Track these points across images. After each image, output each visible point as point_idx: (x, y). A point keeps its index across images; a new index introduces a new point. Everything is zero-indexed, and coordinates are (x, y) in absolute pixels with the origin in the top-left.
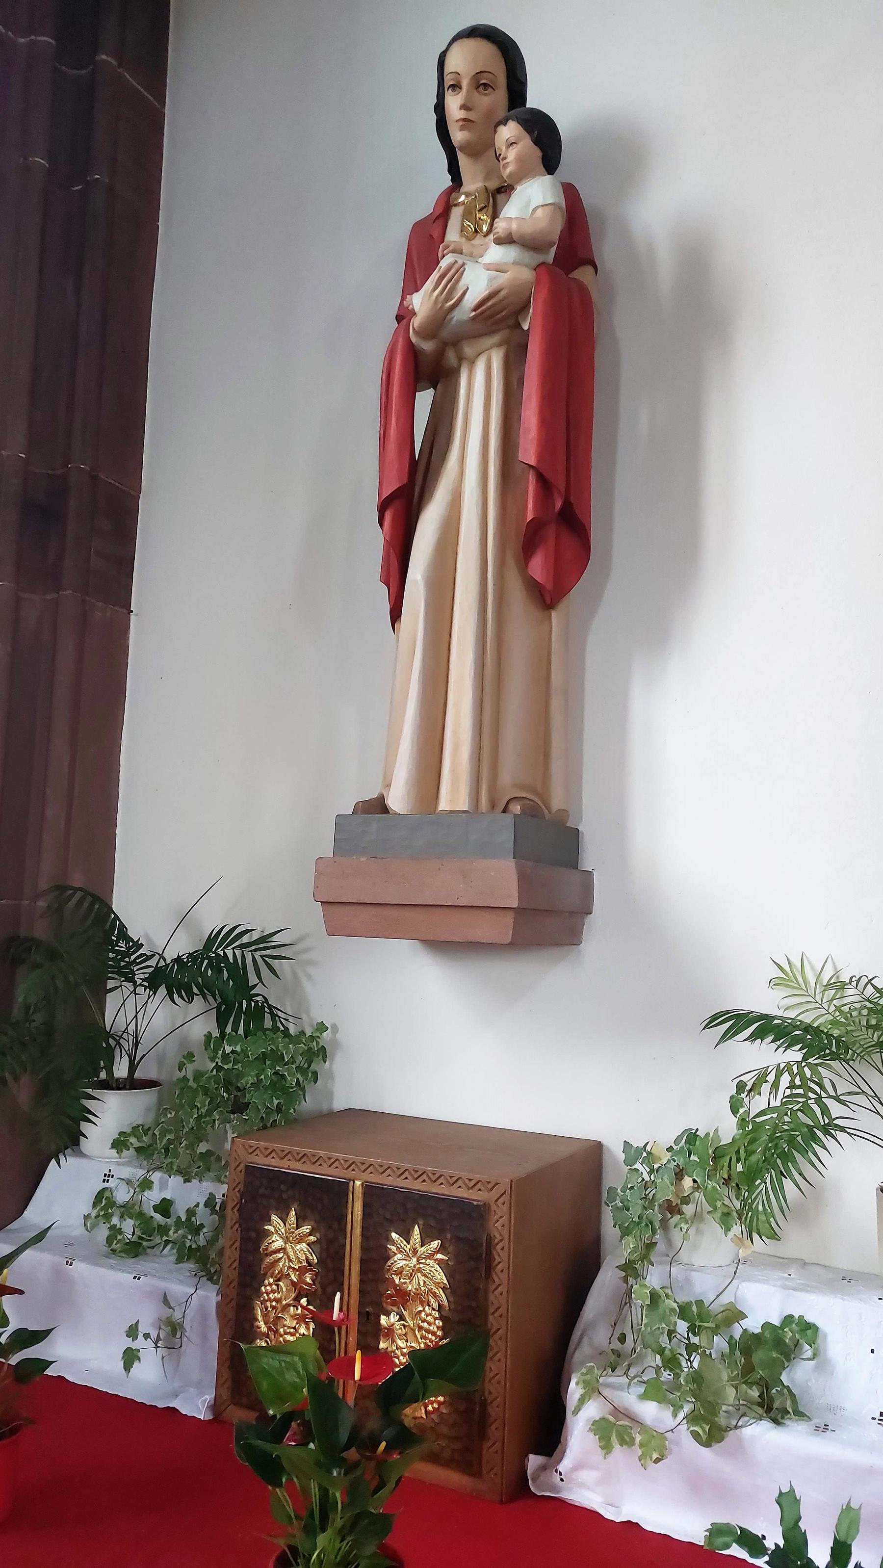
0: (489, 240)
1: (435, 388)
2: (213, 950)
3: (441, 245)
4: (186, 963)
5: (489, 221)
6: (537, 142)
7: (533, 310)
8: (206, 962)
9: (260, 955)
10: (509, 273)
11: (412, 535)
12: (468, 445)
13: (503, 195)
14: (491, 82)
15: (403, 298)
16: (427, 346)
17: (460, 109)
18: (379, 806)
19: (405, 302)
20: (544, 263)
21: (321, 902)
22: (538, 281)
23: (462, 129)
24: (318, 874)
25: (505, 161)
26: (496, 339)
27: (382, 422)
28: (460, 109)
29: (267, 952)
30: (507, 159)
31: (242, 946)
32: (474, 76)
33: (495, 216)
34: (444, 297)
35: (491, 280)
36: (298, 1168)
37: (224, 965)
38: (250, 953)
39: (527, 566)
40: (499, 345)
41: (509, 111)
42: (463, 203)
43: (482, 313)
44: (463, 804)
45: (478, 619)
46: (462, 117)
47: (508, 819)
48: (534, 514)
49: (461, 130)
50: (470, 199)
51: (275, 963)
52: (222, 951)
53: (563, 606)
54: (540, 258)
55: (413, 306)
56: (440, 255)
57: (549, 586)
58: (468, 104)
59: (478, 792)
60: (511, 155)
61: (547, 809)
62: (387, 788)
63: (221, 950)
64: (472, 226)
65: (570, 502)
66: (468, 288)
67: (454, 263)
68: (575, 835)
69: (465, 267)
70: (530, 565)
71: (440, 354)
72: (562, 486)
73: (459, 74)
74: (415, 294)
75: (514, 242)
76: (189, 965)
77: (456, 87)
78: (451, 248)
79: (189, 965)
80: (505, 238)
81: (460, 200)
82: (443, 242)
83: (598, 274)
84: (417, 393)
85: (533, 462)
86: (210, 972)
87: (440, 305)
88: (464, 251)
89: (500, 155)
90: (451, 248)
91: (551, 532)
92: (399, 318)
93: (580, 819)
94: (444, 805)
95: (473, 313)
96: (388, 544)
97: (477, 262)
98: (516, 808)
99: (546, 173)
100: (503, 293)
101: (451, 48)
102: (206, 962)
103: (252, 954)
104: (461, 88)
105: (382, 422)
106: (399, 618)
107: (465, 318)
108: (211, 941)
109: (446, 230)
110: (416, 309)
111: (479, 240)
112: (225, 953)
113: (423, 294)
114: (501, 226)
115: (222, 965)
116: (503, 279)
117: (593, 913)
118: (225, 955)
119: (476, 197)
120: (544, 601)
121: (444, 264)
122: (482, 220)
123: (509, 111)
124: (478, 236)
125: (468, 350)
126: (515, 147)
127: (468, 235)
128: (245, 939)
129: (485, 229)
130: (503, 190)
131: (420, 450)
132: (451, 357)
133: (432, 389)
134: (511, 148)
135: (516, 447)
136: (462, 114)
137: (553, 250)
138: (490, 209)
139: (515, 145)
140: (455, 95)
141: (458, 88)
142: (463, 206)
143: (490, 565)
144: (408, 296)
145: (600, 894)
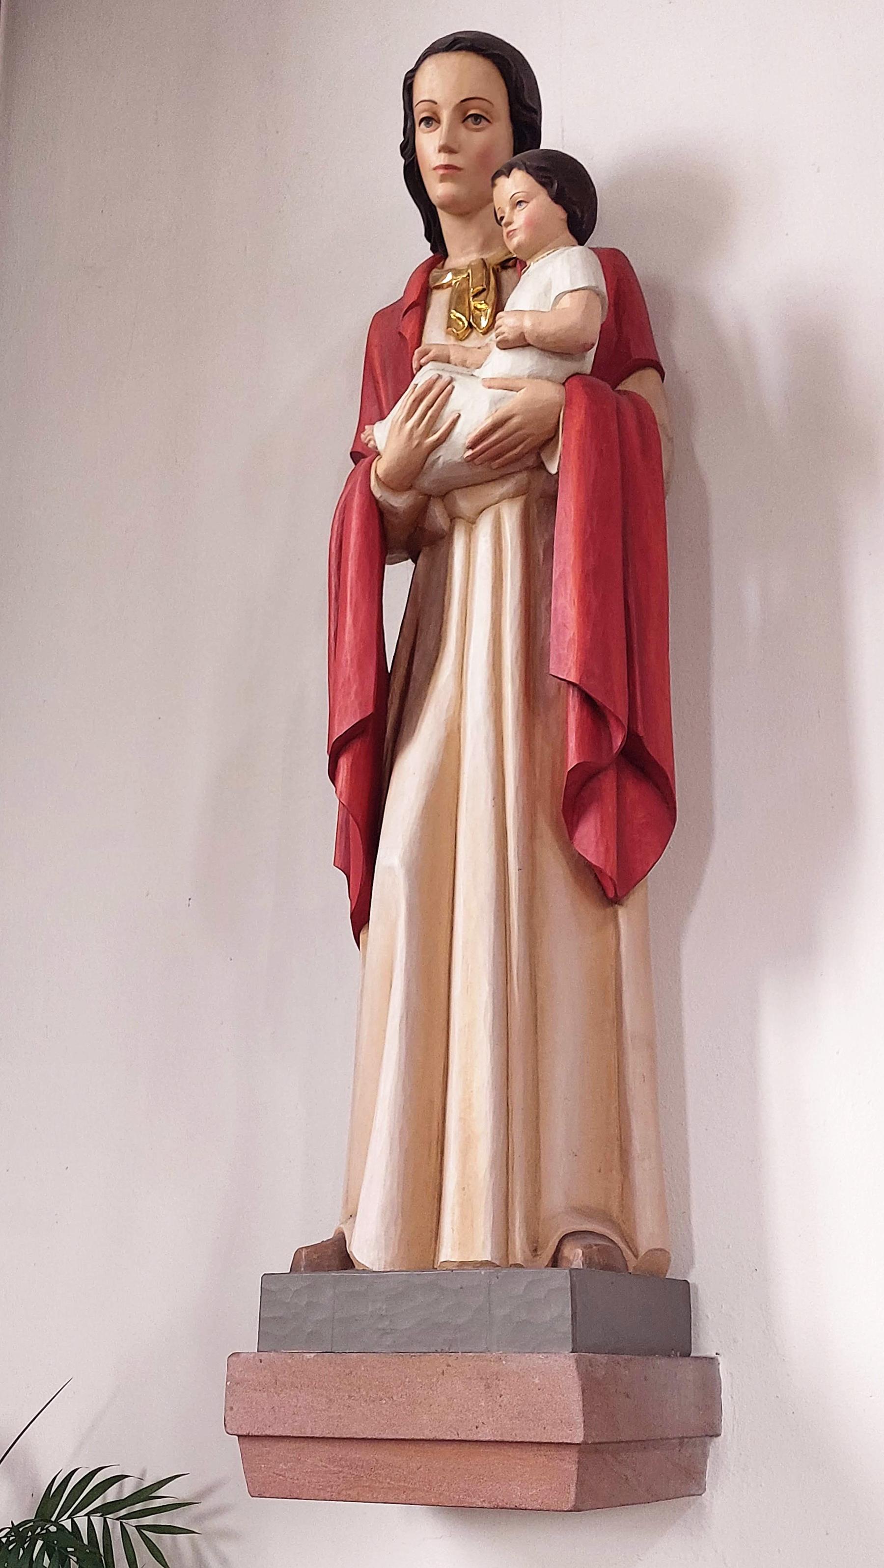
0: (491, 340)
1: (415, 561)
2: (53, 1519)
3: (416, 351)
4: (6, 1546)
5: (489, 311)
6: (557, 198)
7: (563, 446)
8: (40, 1543)
9: (136, 1527)
10: (523, 391)
11: (385, 792)
12: (469, 649)
13: (510, 271)
14: (487, 113)
15: (360, 429)
16: (400, 502)
17: (440, 151)
18: (339, 1245)
19: (362, 436)
20: (577, 374)
21: (239, 1436)
22: (569, 402)
23: (443, 179)
24: (233, 1385)
25: (510, 228)
26: (507, 487)
27: (332, 616)
28: (440, 151)
29: (148, 1520)
30: (513, 225)
31: (106, 1510)
32: (457, 105)
33: (499, 306)
34: (423, 430)
35: (495, 402)
36: (412, 1437)
37: (72, 1550)
38: (118, 1522)
39: (571, 837)
40: (513, 496)
41: (515, 154)
42: (449, 285)
43: (483, 452)
44: (483, 1250)
45: (495, 930)
46: (442, 163)
47: (560, 1278)
48: (579, 758)
49: (441, 181)
50: (460, 278)
51: (164, 1541)
52: (70, 1520)
53: (635, 898)
54: (572, 367)
55: (375, 441)
56: (415, 366)
57: (610, 869)
58: (454, 146)
59: (508, 1229)
60: (520, 218)
61: (630, 1249)
62: (351, 1219)
63: (68, 1518)
64: (463, 318)
65: (638, 736)
66: (459, 416)
67: (437, 379)
68: (684, 1289)
69: (454, 383)
70: (577, 836)
71: (421, 511)
72: (623, 713)
73: (436, 103)
74: (377, 424)
75: (529, 345)
76: (10, 1548)
77: (431, 120)
78: (431, 355)
79: (10, 1548)
80: (514, 340)
81: (445, 281)
82: (420, 346)
83: (665, 381)
84: (386, 566)
85: (572, 678)
86: (46, 1561)
87: (416, 442)
88: (451, 358)
89: (502, 218)
90: (431, 355)
91: (608, 783)
92: (356, 456)
93: (690, 1263)
94: (448, 1252)
95: (470, 452)
96: (347, 809)
97: (472, 375)
98: (575, 1255)
99: (575, 241)
100: (515, 421)
101: (422, 65)
102: (40, 1543)
103: (121, 1523)
104: (439, 122)
105: (332, 616)
106: (367, 925)
107: (457, 458)
108: (50, 1499)
109: (423, 328)
110: (381, 448)
111: (474, 340)
112: (74, 1524)
113: (389, 424)
114: (507, 323)
115: (69, 1549)
116: (512, 401)
117: (722, 1435)
118: (75, 1530)
119: (469, 275)
120: (605, 894)
121: (421, 379)
122: (479, 310)
123: (515, 154)
124: (474, 334)
125: (464, 504)
126: (523, 207)
127: (458, 332)
128: (111, 1495)
129: (484, 323)
130: (511, 263)
131: (394, 657)
132: (438, 515)
133: (410, 560)
134: (518, 208)
135: (545, 656)
136: (442, 159)
137: (591, 355)
138: (492, 295)
139: (524, 205)
140: (431, 132)
141: (434, 122)
142: (450, 289)
143: (512, 836)
144: (366, 427)
145: (732, 1397)
